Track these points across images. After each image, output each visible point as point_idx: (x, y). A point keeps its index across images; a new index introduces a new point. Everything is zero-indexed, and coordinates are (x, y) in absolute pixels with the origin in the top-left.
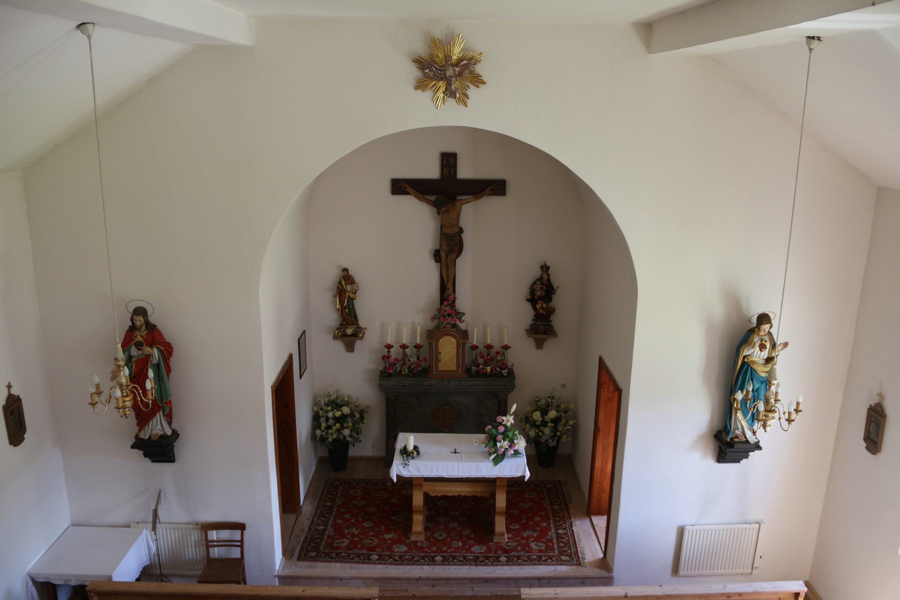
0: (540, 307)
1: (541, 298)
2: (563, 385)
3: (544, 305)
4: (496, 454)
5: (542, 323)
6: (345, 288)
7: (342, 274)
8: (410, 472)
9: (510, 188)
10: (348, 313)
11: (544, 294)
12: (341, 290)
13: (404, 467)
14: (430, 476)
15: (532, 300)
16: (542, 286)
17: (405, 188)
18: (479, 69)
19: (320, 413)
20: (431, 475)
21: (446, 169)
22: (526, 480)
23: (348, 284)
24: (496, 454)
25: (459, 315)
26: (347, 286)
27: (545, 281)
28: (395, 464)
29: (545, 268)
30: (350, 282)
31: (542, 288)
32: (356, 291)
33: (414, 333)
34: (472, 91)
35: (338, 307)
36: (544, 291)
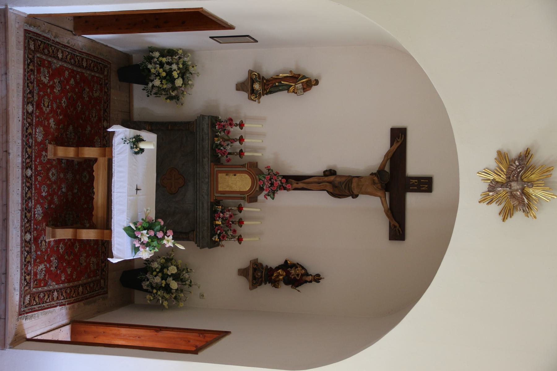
0: (279, 273)
1: (288, 273)
2: (203, 296)
3: (281, 277)
4: (135, 229)
5: (263, 276)
6: (299, 82)
7: (313, 79)
8: (117, 145)
9: (397, 244)
10: (274, 85)
11: (293, 277)
12: (297, 78)
13: (123, 139)
14: (113, 164)
15: (287, 266)
16: (300, 275)
17: (398, 142)
18: (519, 215)
19: (176, 56)
20: (114, 166)
21: (416, 182)
22: (109, 259)
23: (302, 85)
24: (135, 229)
25: (272, 194)
26: (301, 84)
27: (305, 278)
28: (126, 131)
29: (317, 278)
30: (305, 87)
31: (298, 275)
32: (296, 93)
33: (255, 150)
34: (495, 208)
35: (280, 75)
36: (295, 277)
